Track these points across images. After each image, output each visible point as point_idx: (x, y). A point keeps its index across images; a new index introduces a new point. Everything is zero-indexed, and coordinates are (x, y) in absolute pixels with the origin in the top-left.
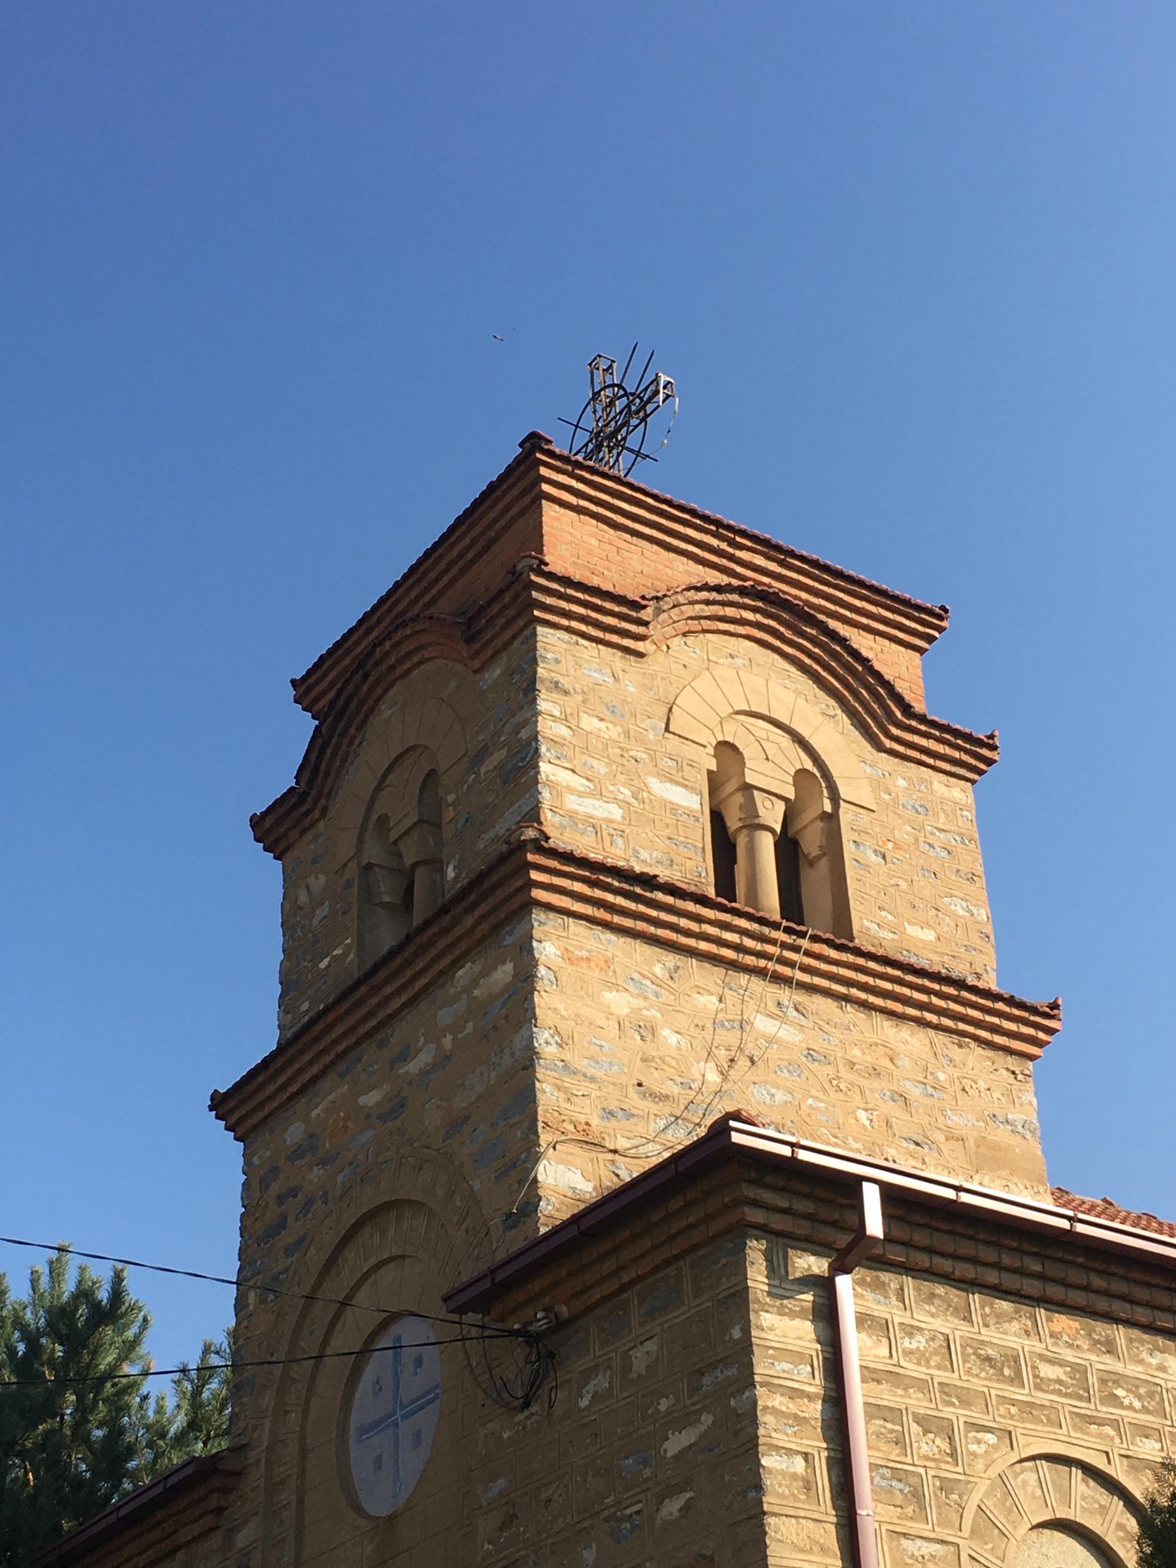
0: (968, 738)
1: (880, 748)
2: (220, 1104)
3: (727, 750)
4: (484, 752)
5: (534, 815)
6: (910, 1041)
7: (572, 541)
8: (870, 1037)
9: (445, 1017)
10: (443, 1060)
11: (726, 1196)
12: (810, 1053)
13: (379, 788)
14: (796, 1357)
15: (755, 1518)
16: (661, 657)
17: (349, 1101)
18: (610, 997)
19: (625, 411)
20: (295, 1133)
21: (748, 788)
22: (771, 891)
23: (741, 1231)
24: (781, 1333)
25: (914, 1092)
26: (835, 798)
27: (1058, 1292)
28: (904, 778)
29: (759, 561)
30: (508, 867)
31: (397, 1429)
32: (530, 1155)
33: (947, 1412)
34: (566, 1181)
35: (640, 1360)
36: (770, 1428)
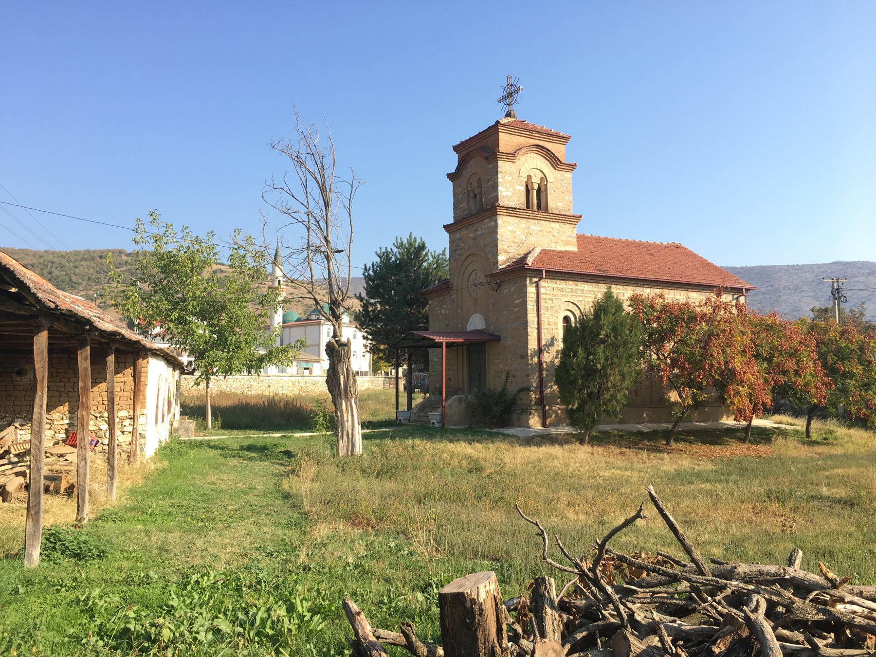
3: (529, 177)
6: (556, 225)
7: (506, 141)
9: (483, 227)
10: (483, 234)
11: (520, 270)
17: (467, 234)
20: (458, 236)
22: (537, 201)
23: (527, 277)
24: (531, 290)
25: (556, 234)
28: (559, 174)
35: (512, 289)
36: (528, 303)
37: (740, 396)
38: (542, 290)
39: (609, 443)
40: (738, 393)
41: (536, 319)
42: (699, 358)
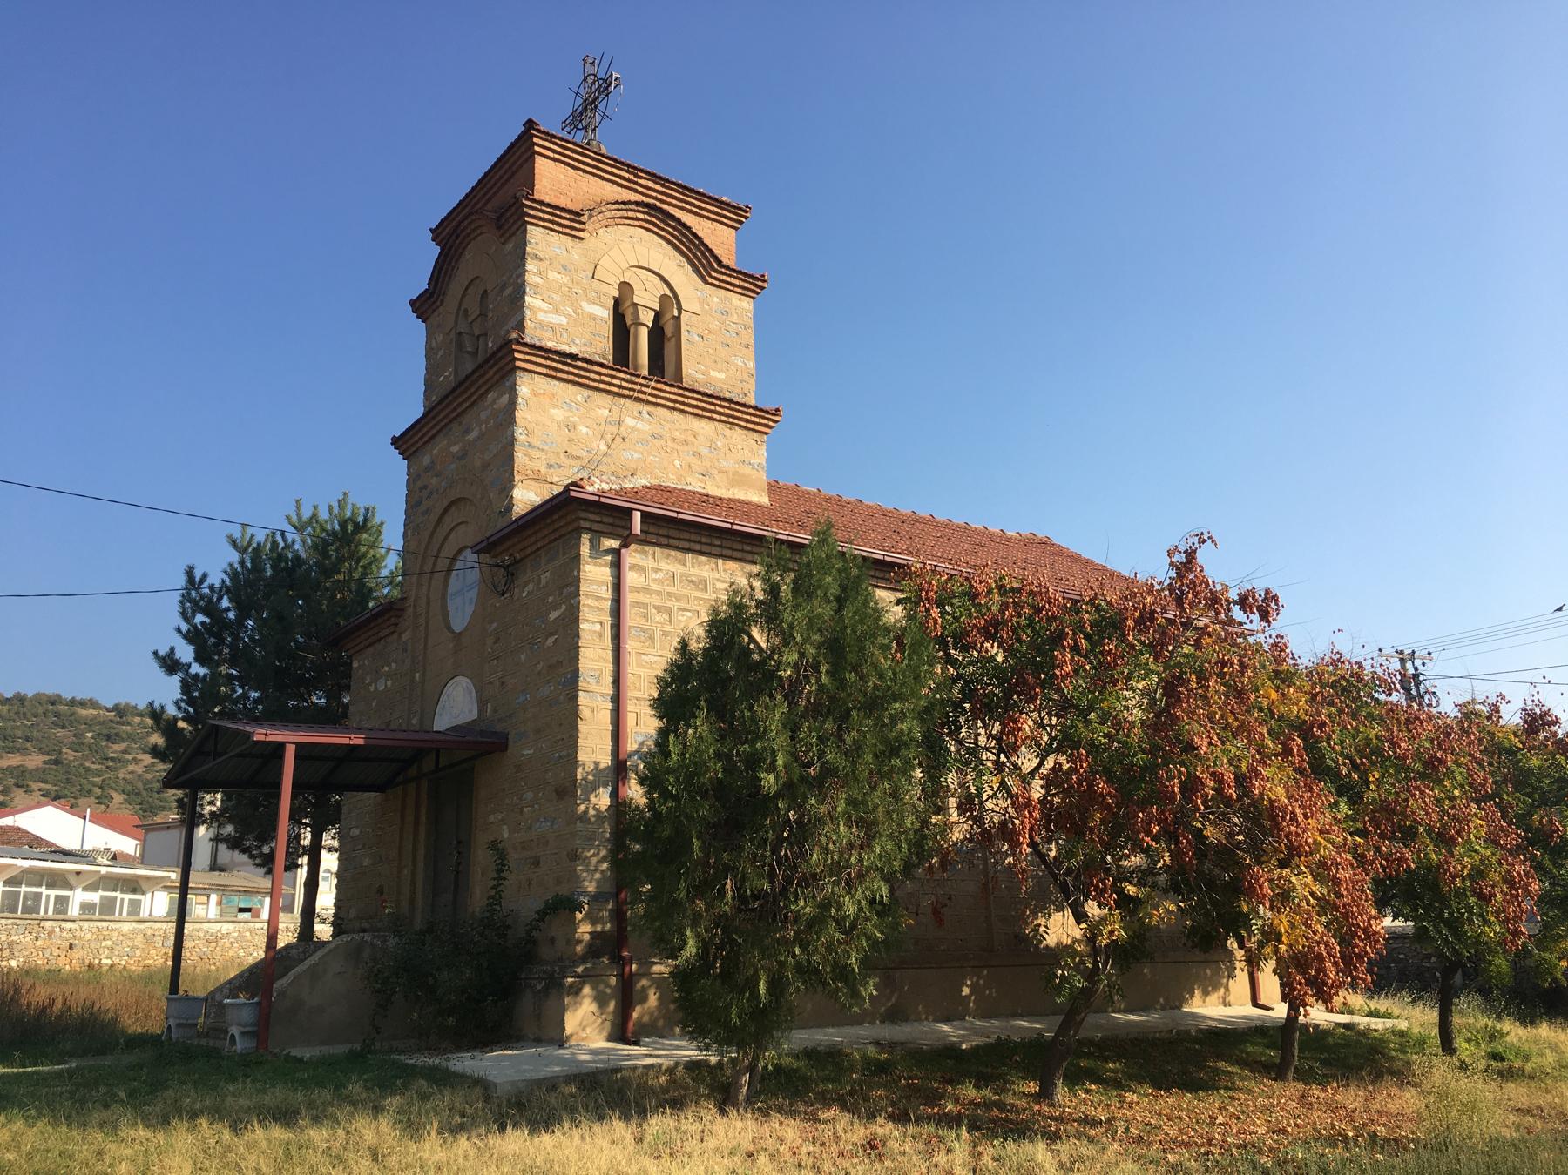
0: (751, 276)
1: (706, 282)
2: (396, 442)
3: (625, 287)
4: (504, 287)
5: (521, 326)
6: (704, 428)
7: (553, 179)
8: (684, 426)
10: (481, 436)
11: (574, 515)
12: (653, 435)
13: (464, 295)
14: (600, 583)
15: (576, 648)
16: (593, 240)
17: (445, 447)
18: (554, 411)
19: (594, 95)
20: (426, 460)
21: (635, 305)
22: (643, 354)
23: (579, 531)
24: (594, 575)
25: (704, 451)
26: (680, 309)
27: (729, 553)
28: (716, 297)
29: (651, 184)
30: (504, 351)
31: (463, 596)
32: (508, 485)
33: (669, 604)
34: (526, 497)
36: (585, 612)
37: (1292, 900)
38: (631, 578)
39: (826, 1101)
40: (1284, 897)
41: (610, 667)
42: (1141, 758)
